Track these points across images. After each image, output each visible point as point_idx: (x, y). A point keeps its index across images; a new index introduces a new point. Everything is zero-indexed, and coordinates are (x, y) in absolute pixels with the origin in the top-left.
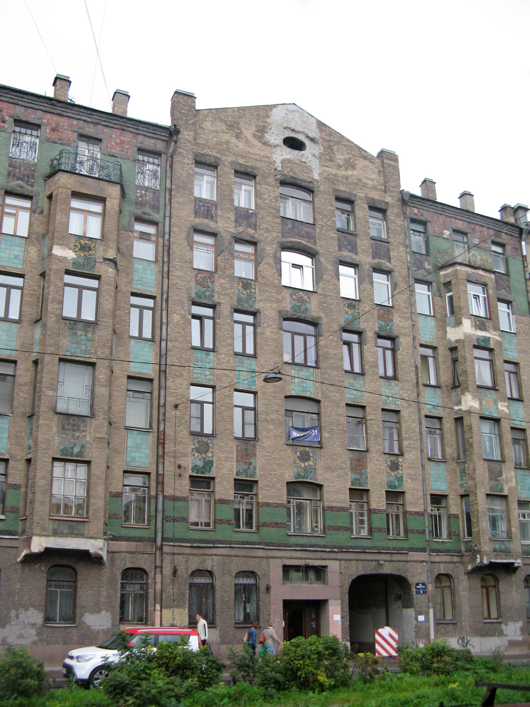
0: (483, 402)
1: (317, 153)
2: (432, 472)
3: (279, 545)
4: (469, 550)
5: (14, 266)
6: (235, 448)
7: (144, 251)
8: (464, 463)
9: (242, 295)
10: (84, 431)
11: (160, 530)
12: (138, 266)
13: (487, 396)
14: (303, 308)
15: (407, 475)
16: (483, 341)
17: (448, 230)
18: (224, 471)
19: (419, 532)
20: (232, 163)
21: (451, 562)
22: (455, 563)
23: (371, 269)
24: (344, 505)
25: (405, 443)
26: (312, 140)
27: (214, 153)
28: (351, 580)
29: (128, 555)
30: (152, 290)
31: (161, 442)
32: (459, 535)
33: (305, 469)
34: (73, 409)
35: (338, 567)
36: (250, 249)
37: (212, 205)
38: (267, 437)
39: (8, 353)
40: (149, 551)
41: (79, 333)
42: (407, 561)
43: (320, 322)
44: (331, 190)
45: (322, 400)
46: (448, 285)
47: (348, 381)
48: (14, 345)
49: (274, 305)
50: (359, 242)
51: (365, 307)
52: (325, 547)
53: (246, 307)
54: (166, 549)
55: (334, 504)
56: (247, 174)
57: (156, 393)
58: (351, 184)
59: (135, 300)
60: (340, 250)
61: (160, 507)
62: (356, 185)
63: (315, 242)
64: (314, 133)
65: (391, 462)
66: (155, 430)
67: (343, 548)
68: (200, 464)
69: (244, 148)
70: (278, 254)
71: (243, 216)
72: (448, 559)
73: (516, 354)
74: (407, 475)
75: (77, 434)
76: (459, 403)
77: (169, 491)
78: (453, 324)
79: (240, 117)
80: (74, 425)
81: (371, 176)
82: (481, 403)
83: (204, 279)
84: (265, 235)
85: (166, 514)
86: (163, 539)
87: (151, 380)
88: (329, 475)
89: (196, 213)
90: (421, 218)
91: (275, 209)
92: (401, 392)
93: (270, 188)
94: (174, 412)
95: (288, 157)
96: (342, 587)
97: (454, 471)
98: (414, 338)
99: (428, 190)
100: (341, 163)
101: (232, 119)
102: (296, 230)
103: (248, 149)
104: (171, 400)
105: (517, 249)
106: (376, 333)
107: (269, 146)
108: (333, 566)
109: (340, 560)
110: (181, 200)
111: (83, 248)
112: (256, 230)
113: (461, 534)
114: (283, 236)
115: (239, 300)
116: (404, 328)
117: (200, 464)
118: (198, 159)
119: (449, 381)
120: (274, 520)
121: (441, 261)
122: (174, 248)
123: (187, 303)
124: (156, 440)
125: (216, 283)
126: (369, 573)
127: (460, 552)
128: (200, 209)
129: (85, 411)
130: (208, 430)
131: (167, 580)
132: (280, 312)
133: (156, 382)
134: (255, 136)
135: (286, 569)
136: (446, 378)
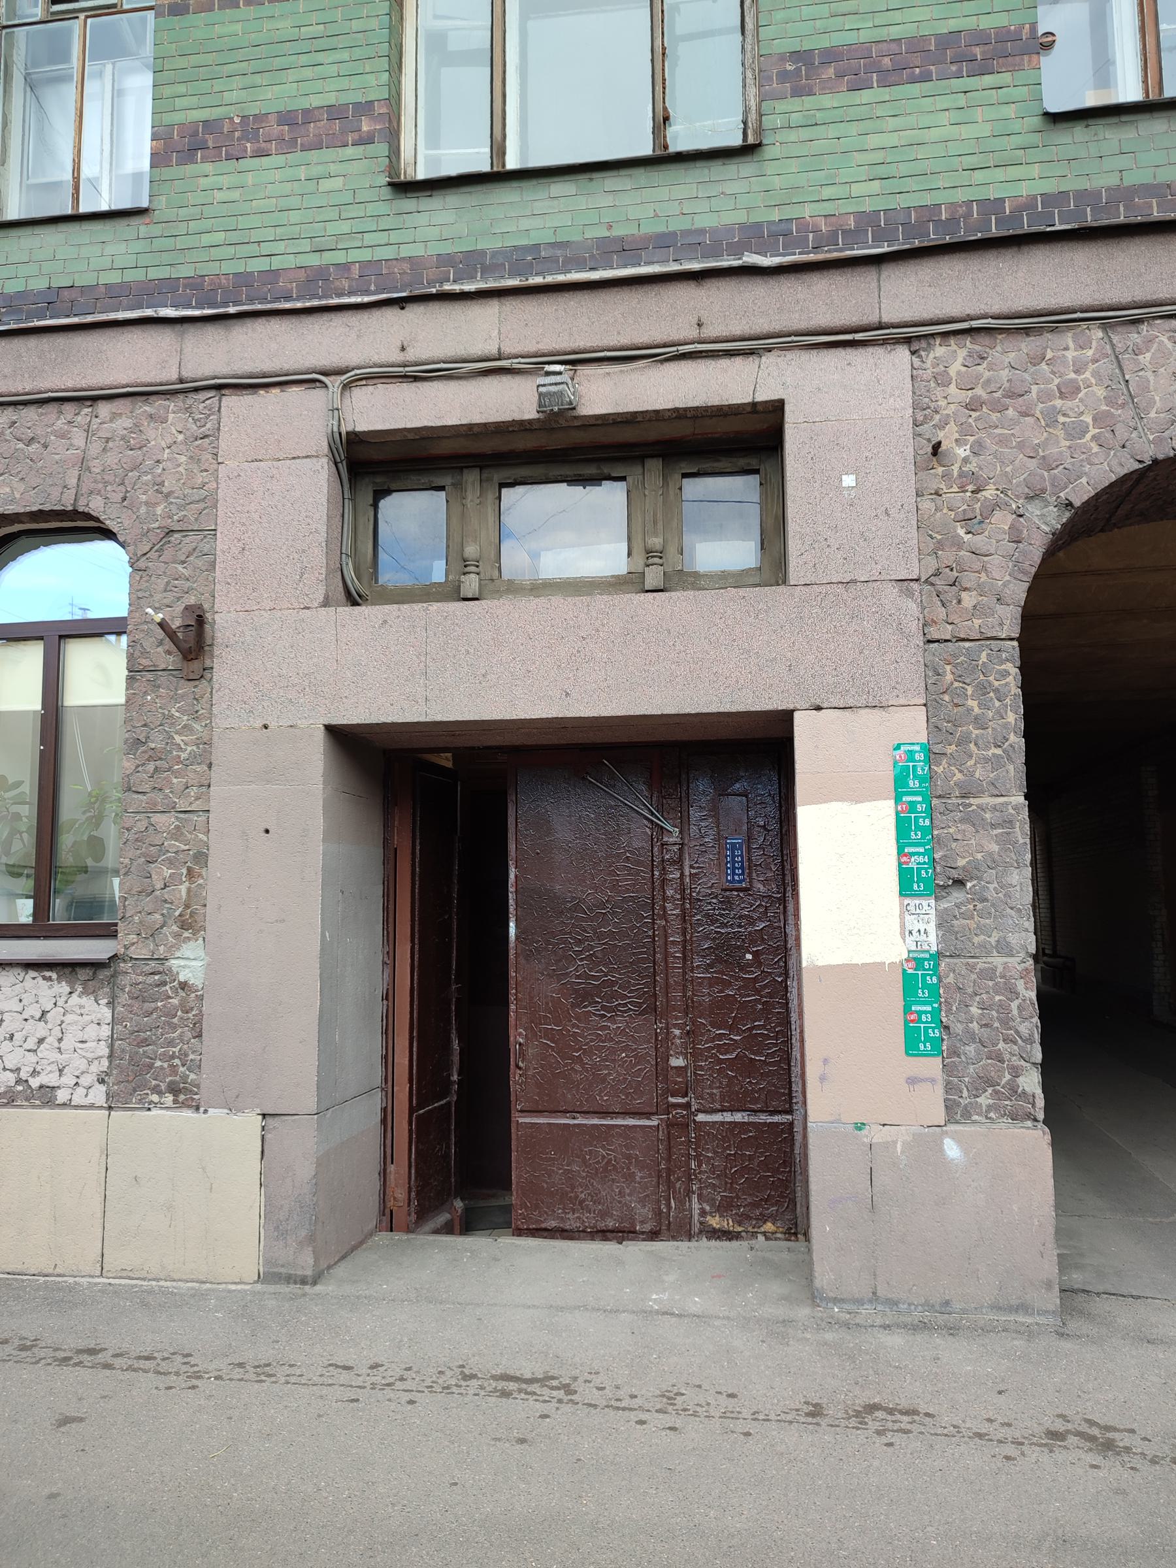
28: (1046, 520)
35: (901, 406)
96: (940, 583)
99: (685, 921)
108: (849, 420)
109: (912, 336)
135: (372, 466)
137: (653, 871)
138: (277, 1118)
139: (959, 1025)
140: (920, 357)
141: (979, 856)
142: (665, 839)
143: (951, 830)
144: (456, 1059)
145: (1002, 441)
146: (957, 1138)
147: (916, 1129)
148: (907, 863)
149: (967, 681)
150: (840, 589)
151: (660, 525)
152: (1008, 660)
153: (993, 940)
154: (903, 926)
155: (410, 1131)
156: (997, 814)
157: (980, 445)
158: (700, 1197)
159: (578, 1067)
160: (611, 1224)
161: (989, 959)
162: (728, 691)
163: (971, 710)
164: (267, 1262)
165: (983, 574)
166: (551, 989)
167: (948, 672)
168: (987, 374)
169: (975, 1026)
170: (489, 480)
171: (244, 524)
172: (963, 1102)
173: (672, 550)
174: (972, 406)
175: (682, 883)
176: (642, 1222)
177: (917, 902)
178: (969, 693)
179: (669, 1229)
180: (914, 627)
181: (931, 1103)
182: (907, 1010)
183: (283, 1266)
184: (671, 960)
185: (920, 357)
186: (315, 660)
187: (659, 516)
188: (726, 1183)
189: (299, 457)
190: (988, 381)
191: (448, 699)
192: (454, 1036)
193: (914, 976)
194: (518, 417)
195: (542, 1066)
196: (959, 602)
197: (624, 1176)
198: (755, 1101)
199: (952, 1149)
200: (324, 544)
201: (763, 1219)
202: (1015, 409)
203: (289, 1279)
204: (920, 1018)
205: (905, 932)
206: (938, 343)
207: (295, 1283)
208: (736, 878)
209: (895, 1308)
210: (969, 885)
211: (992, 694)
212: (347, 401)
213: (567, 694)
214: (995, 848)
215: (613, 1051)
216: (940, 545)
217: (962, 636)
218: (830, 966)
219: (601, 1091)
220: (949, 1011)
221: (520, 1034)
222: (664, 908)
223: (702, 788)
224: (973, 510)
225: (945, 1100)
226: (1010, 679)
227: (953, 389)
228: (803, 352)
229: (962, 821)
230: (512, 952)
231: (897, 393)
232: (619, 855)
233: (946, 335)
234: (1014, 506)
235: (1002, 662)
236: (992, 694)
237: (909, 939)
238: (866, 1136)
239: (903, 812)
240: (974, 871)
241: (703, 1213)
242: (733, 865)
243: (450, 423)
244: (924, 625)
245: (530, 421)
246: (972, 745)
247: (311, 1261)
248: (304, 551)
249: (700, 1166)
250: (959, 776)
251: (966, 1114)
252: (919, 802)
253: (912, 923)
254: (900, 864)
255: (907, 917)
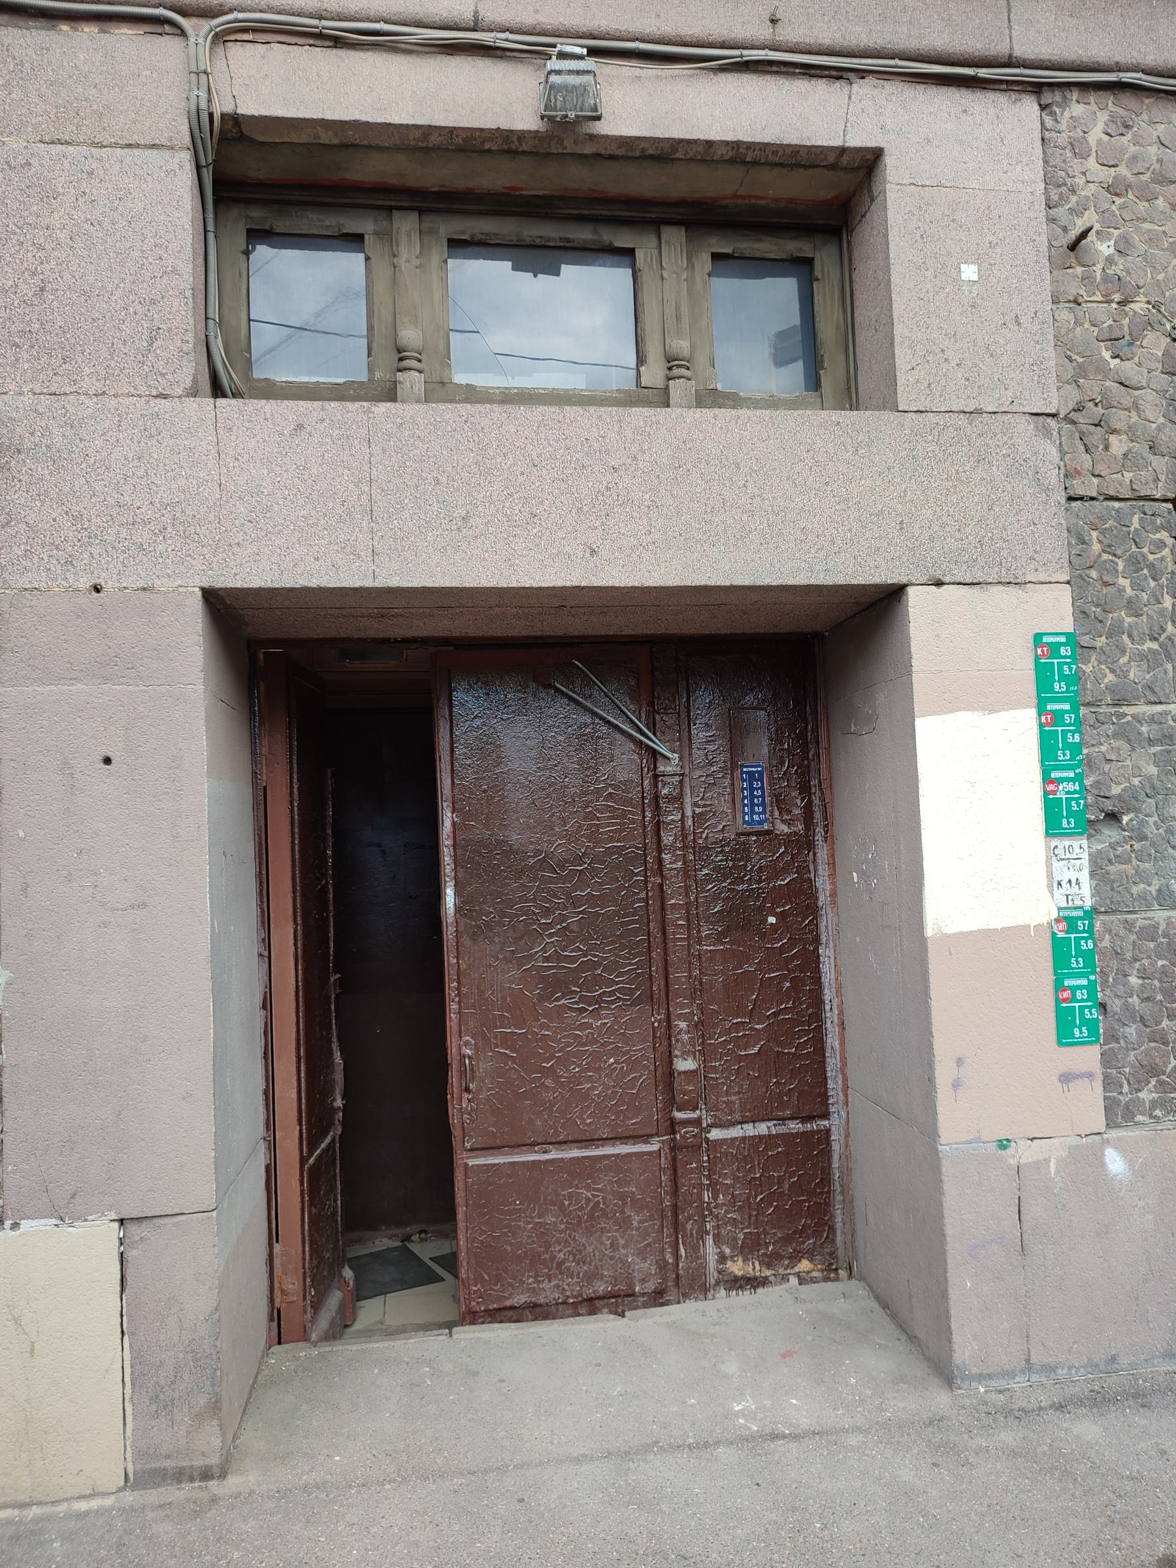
35: (1029, 176)
135: (263, 183)
137: (644, 812)
138: (145, 1224)
139: (1116, 1001)
140: (1053, 114)
141: (1136, 781)
142: (661, 768)
143: (1103, 748)
144: (339, 1076)
145: (1152, 240)
146: (1120, 1146)
147: (1073, 1141)
148: (1054, 792)
149: (1119, 552)
150: (962, 421)
151: (686, 322)
152: (1163, 527)
153: (1153, 889)
154: (1050, 875)
155: (302, 1192)
156: (1155, 726)
157: (1127, 242)
158: (717, 1239)
159: (549, 1082)
160: (601, 1288)
161: (1149, 914)
162: (821, 555)
163: (1121, 590)
164: (140, 1454)
165: (1134, 414)
166: (509, 978)
167: (1095, 540)
168: (1133, 149)
169: (1135, 1000)
170: (433, 232)
171: (41, 248)
172: (1123, 1099)
173: (702, 360)
174: (1114, 189)
175: (683, 828)
176: (643, 1281)
177: (1067, 843)
178: (1120, 568)
179: (677, 1285)
180: (1053, 477)
181: (1088, 1104)
182: (1059, 987)
183: (168, 1457)
184: (670, 929)
185: (1053, 114)
186: (182, 482)
187: (685, 309)
188: (750, 1216)
189: (138, 146)
190: (1134, 159)
191: (408, 554)
192: (335, 1046)
193: (1065, 941)
194: (505, 125)
195: (499, 1085)
196: (1107, 448)
197: (617, 1222)
198: (782, 1106)
199: (1115, 1163)
200: (189, 293)
201: (795, 1257)
202: (1166, 200)
203: (180, 1476)
204: (1073, 994)
205: (1054, 884)
206: (1075, 98)
207: (192, 1479)
208: (756, 817)
209: (1053, 1376)
210: (1125, 819)
211: (1145, 571)
212: (220, 63)
213: (593, 552)
214: (1153, 770)
215: (597, 1057)
216: (1082, 371)
217: (1112, 493)
218: (962, 933)
219: (582, 1113)
220: (1105, 983)
221: (467, 1044)
222: (660, 861)
223: (704, 699)
224: (1121, 327)
225: (1105, 1098)
226: (1166, 552)
227: (1091, 163)
228: (906, 85)
229: (1116, 736)
230: (449, 933)
231: (1025, 159)
232: (598, 792)
233: (1084, 87)
234: (1168, 327)
235: (1157, 530)
236: (1145, 571)
237: (1058, 893)
238: (1012, 1156)
239: (1047, 724)
240: (1129, 801)
241: (722, 1259)
242: (752, 801)
243: (396, 120)
244: (1066, 476)
245: (521, 135)
246: (1125, 637)
247: (217, 1442)
248: (153, 302)
249: (715, 1198)
250: (1110, 677)
251: (1129, 1114)
252: (1067, 712)
253: (1062, 872)
254: (1046, 793)
255: (1056, 865)
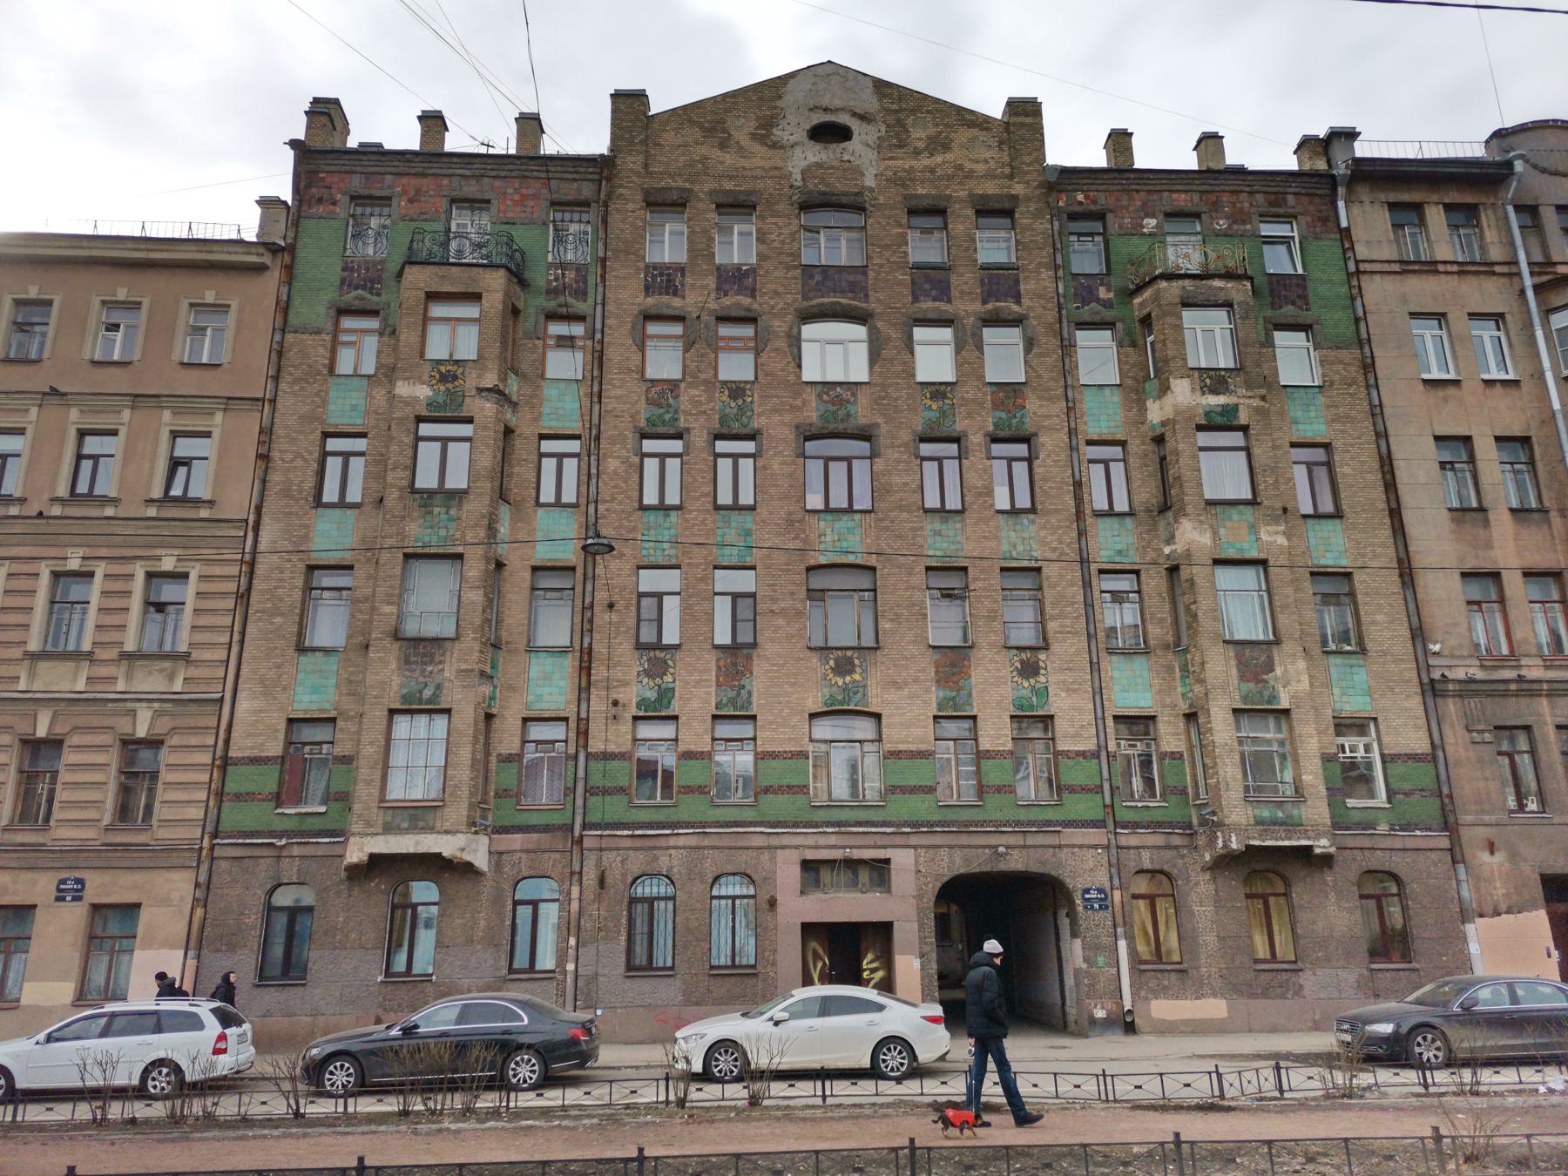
0: (1222, 531)
1: (872, 139)
2: (1116, 674)
3: (796, 825)
4: (1203, 822)
5: (351, 421)
6: (713, 665)
7: (564, 365)
8: (1186, 651)
9: (728, 410)
10: (440, 662)
11: (579, 811)
12: (550, 392)
13: (1231, 519)
14: (842, 413)
15: (1057, 683)
16: (1222, 414)
17: (1153, 216)
18: (695, 704)
19: (1085, 790)
20: (711, 193)
21: (1167, 847)
22: (1176, 847)
23: (979, 323)
24: (923, 747)
25: (1052, 626)
26: (863, 117)
27: (680, 183)
28: (939, 885)
29: (524, 856)
30: (575, 425)
31: (585, 668)
32: (1184, 792)
33: (845, 688)
34: (431, 629)
35: (912, 860)
36: (748, 331)
37: (676, 270)
38: (772, 640)
39: (339, 555)
40: (560, 847)
41: (436, 510)
42: (1060, 847)
43: (874, 432)
44: (900, 198)
45: (879, 567)
46: (1146, 321)
47: (929, 527)
48: (349, 542)
49: (788, 418)
50: (954, 279)
51: (969, 392)
52: (885, 824)
53: (736, 427)
54: (587, 843)
55: (903, 747)
56: (736, 205)
57: (579, 589)
58: (940, 179)
59: (547, 446)
60: (916, 299)
61: (581, 773)
62: (950, 178)
63: (867, 296)
64: (869, 102)
65: (1022, 662)
66: (577, 647)
67: (922, 825)
68: (652, 695)
69: (743, 161)
70: (795, 331)
71: (734, 278)
72: (1159, 840)
73: (1323, 427)
74: (1057, 683)
75: (429, 668)
76: (1170, 540)
77: (596, 745)
78: (1155, 393)
79: (727, 111)
80: (424, 655)
81: (985, 156)
82: (1215, 533)
83: (661, 394)
84: (772, 302)
85: (591, 783)
86: (585, 826)
87: (573, 569)
88: (892, 695)
89: (647, 288)
90: (1092, 207)
91: (792, 255)
92: (1042, 533)
93: (781, 221)
94: (607, 617)
95: (812, 159)
96: (919, 897)
97: (1170, 669)
98: (1072, 432)
100: (921, 145)
101: (710, 117)
102: (829, 284)
103: (743, 162)
104: (602, 596)
105: (1325, 220)
106: (987, 435)
107: (782, 147)
108: (902, 860)
109: (915, 847)
110: (622, 272)
111: (444, 378)
112: (754, 297)
113: (1190, 791)
114: (805, 298)
115: (723, 419)
116: (1049, 417)
117: (652, 695)
118: (651, 199)
119: (1154, 501)
120: (785, 782)
121: (1131, 282)
122: (610, 353)
123: (631, 437)
124: (577, 663)
125: (683, 398)
126: (978, 870)
127: (1190, 826)
128: (654, 281)
129: (449, 631)
130: (671, 636)
131: (589, 894)
132: (797, 427)
133: (580, 571)
134: (754, 136)
135: (807, 865)
136: (1148, 494)
